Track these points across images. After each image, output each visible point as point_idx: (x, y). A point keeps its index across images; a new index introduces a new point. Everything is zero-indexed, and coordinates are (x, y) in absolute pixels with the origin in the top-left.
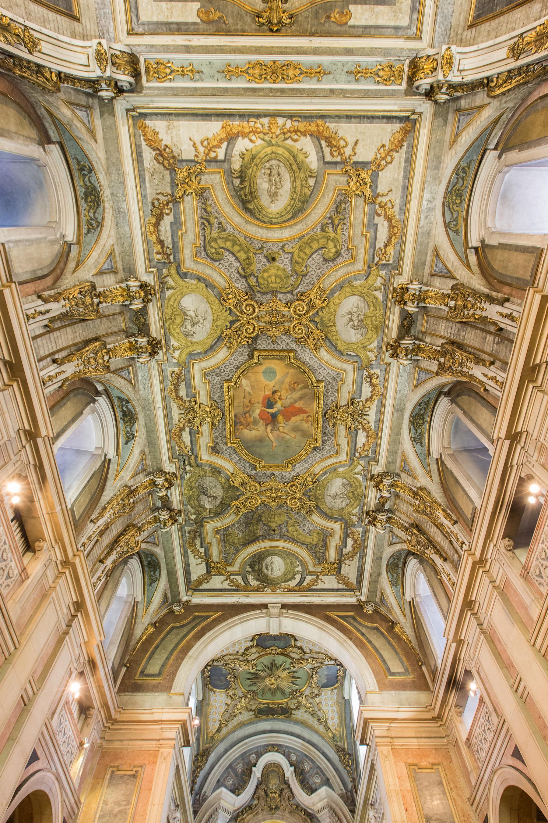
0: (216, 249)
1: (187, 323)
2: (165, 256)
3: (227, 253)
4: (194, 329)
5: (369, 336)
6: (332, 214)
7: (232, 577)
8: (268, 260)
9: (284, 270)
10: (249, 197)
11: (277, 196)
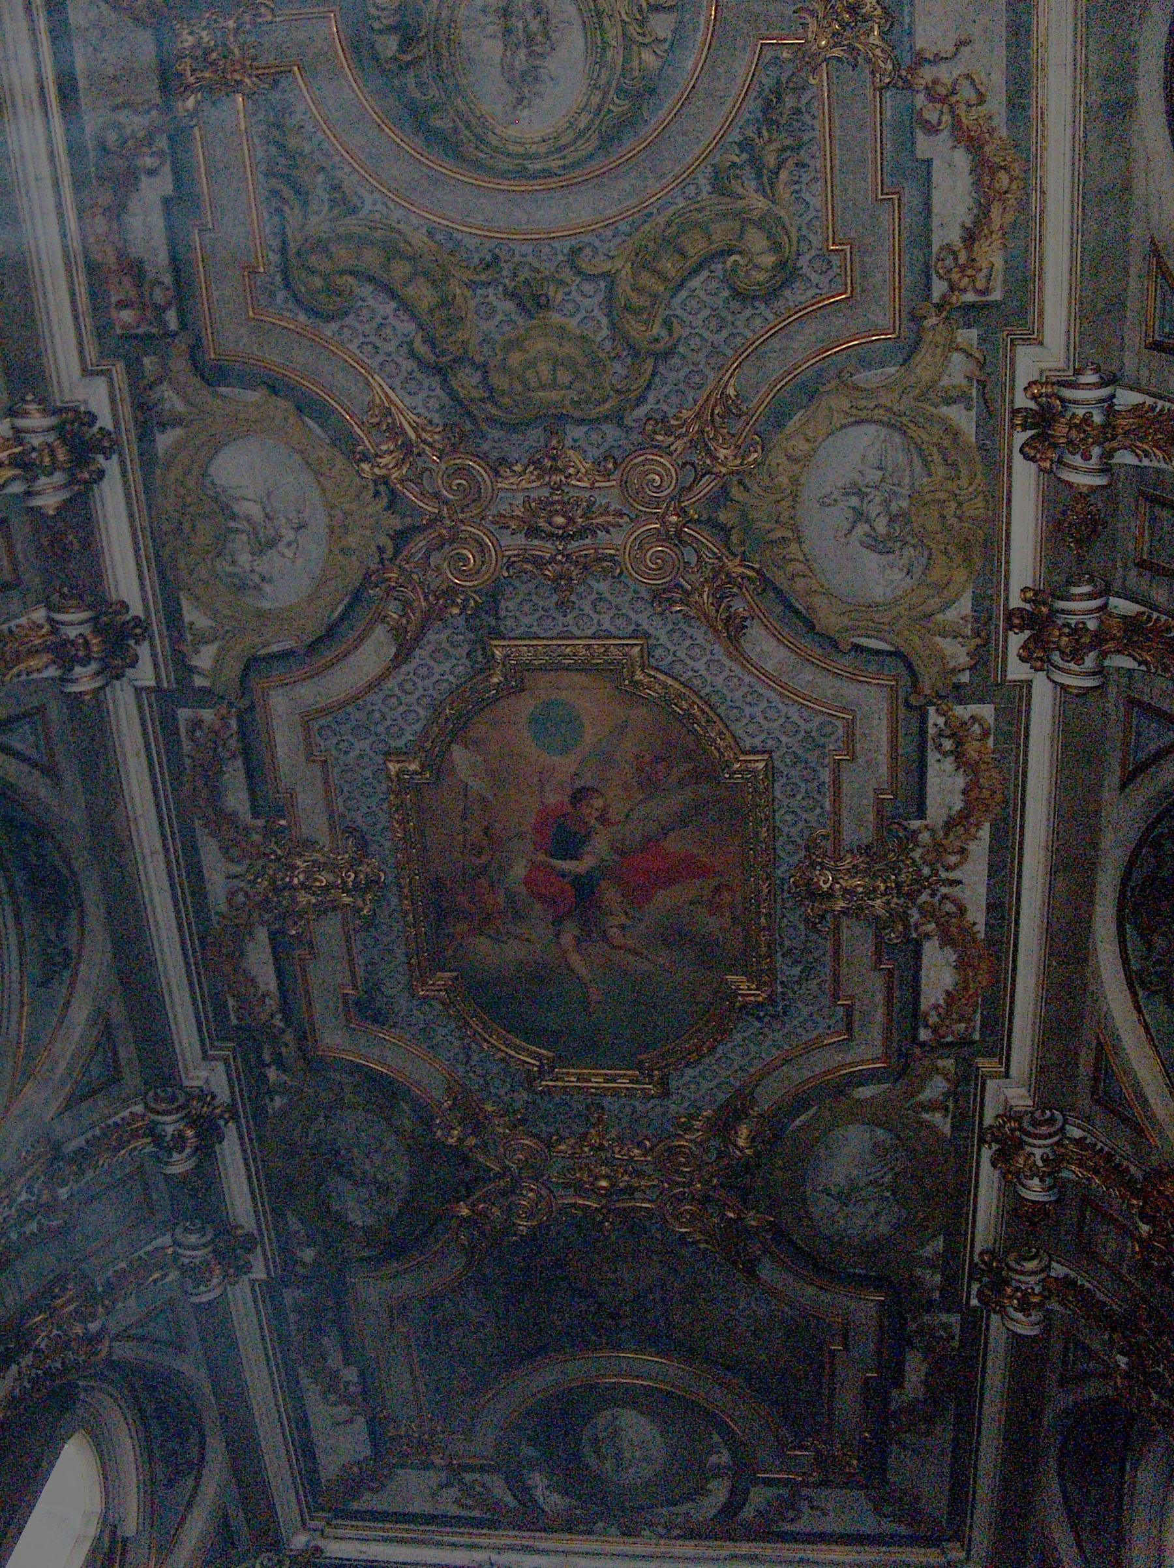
0: (324, 277)
1: (238, 545)
2: (149, 314)
3: (366, 291)
4: (262, 566)
5: (936, 575)
6: (750, 132)
7: (468, 1477)
8: (522, 306)
9: (583, 338)
10: (433, 92)
11: (537, 79)
